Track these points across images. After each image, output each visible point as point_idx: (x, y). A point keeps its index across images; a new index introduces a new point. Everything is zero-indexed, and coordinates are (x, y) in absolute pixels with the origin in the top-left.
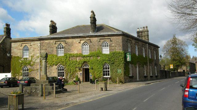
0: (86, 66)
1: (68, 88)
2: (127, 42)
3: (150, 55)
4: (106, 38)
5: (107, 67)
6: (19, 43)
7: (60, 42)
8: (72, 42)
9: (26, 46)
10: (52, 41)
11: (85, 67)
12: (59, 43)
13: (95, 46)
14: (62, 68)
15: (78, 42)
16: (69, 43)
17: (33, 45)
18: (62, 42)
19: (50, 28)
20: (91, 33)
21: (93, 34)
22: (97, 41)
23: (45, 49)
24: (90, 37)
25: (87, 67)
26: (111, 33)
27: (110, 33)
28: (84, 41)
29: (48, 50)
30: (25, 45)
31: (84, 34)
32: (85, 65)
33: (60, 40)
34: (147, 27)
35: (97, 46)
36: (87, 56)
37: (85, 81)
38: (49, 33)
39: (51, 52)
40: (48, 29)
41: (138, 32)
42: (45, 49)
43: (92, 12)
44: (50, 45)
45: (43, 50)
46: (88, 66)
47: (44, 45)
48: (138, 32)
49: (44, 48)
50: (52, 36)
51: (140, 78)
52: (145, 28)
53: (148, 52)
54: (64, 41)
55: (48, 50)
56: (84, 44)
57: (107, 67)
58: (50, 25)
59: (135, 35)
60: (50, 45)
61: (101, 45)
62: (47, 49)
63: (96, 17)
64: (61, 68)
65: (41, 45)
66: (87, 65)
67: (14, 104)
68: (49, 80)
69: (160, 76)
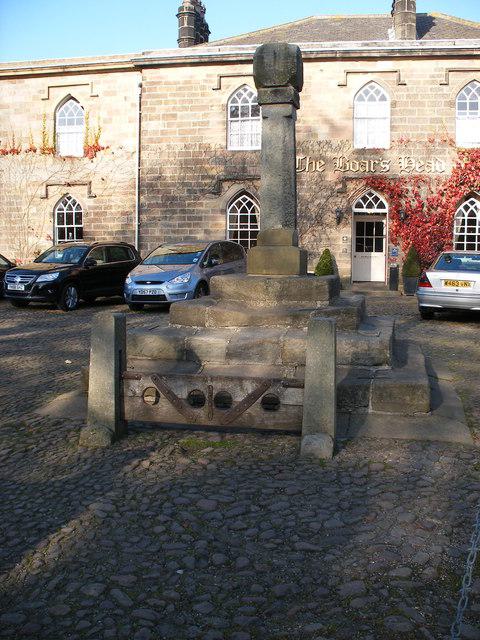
0: (370, 206)
13: (421, 104)
15: (334, 84)
17: (107, 94)
19: (181, 23)
20: (395, 39)
22: (433, 82)
23: (165, 116)
29: (178, 120)
31: (367, 45)
35: (434, 104)
37: (238, 263)
39: (194, 131)
40: (172, 28)
42: (165, 116)
45: (158, 118)
46: (381, 206)
47: (165, 96)
49: (161, 109)
55: (178, 120)
56: (367, 93)
57: (74, 212)
58: (181, 9)
60: (194, 95)
61: (451, 104)
62: (174, 116)
64: (70, 208)
65: (149, 96)
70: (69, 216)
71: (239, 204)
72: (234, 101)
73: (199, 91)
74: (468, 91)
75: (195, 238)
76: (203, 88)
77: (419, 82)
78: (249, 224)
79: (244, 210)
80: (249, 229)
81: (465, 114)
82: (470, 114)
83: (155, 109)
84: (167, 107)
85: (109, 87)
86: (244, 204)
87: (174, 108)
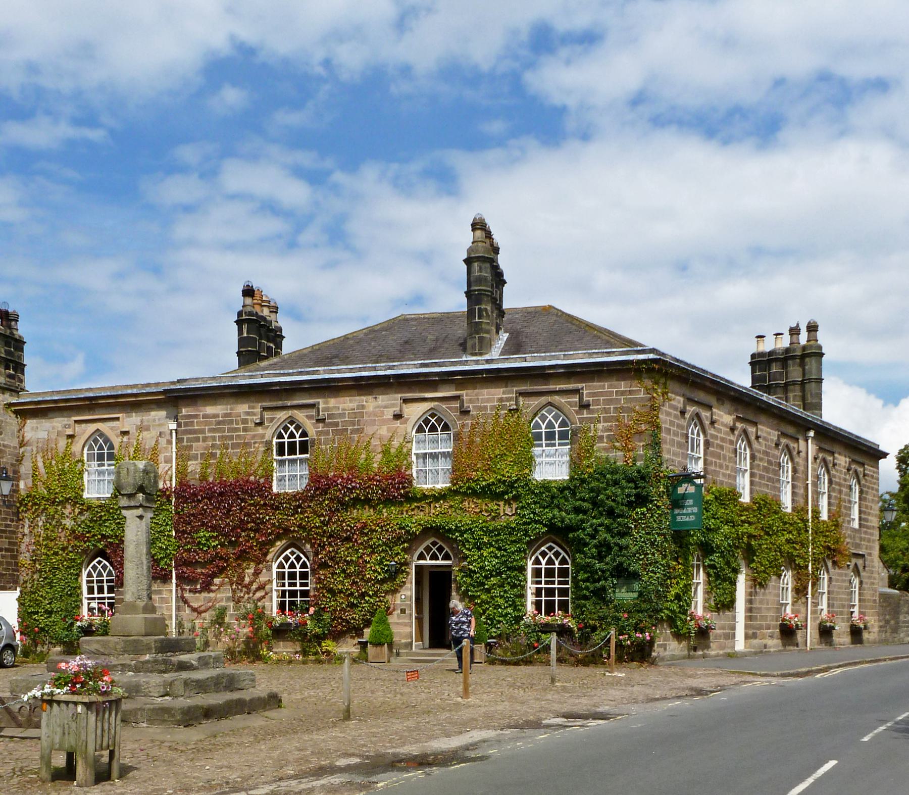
0: (434, 557)
1: (281, 688)
2: (683, 413)
3: (824, 502)
4: (558, 387)
5: (543, 566)
6: (58, 423)
7: (290, 413)
8: (358, 414)
9: (102, 435)
10: (242, 408)
11: (428, 562)
12: (282, 415)
14: (298, 570)
15: (389, 414)
16: (342, 415)
18: (300, 416)
19: (240, 331)
21: (477, 362)
24: (460, 385)
25: (440, 562)
26: (590, 355)
27: (580, 358)
28: (426, 406)
30: (92, 427)
32: (428, 549)
33: (552, 387)
34: (812, 328)
36: (441, 496)
38: (234, 361)
40: (230, 335)
41: (760, 362)
43: (479, 225)
44: (237, 430)
47: (202, 431)
48: (760, 362)
49: (198, 448)
50: (325, 372)
51: (754, 636)
52: (803, 338)
53: (815, 485)
54: (312, 406)
57: (298, 439)
59: (743, 379)
60: (237, 430)
63: (503, 261)
64: (292, 566)
66: (440, 549)
67: (766, 682)
68: (681, 594)
69: (876, 629)
70: (292, 446)
71: (287, 559)
72: (280, 436)
73: (241, 426)
74: (543, 418)
75: (770, 652)
76: (245, 421)
77: (485, 408)
78: (556, 579)
79: (292, 566)
80: (556, 586)
81: (554, 445)
82: (560, 445)
83: (192, 446)
84: (204, 445)
85: (142, 421)
86: (434, 549)
87: (213, 446)
